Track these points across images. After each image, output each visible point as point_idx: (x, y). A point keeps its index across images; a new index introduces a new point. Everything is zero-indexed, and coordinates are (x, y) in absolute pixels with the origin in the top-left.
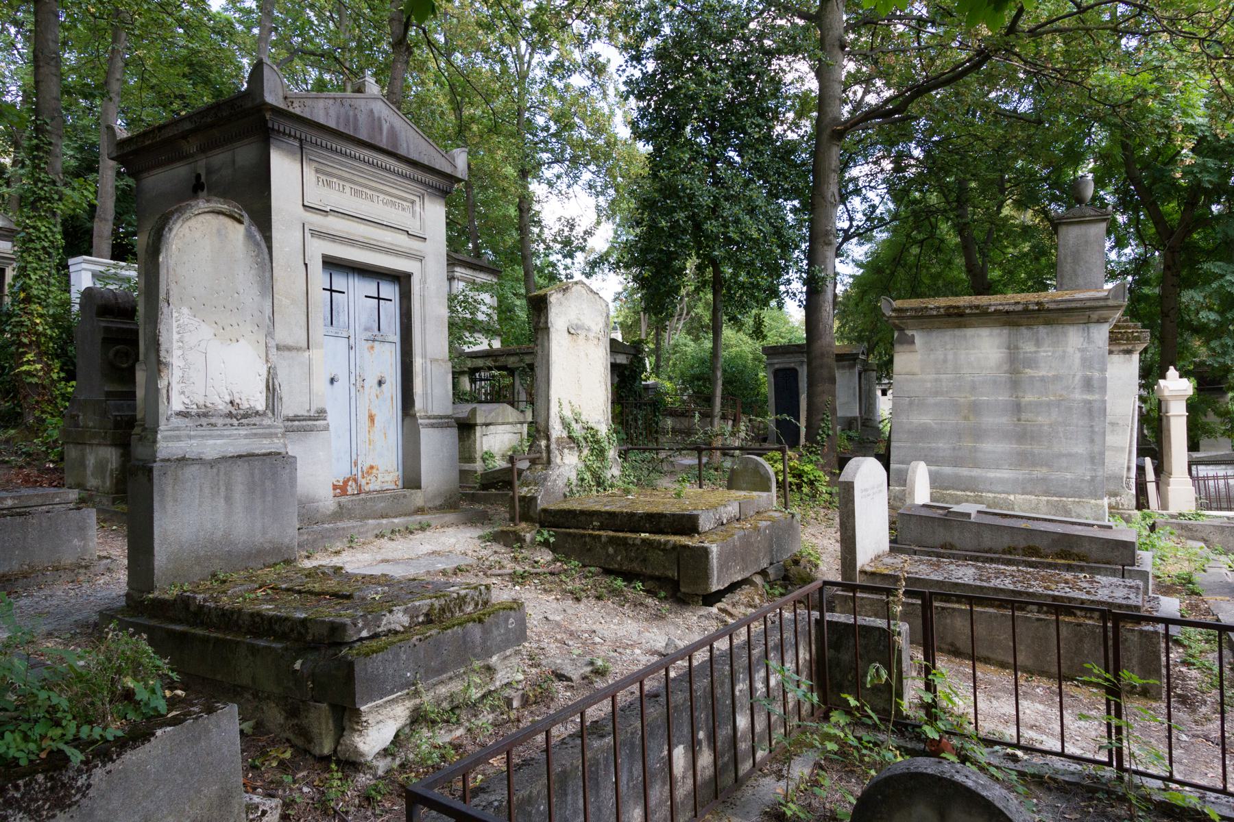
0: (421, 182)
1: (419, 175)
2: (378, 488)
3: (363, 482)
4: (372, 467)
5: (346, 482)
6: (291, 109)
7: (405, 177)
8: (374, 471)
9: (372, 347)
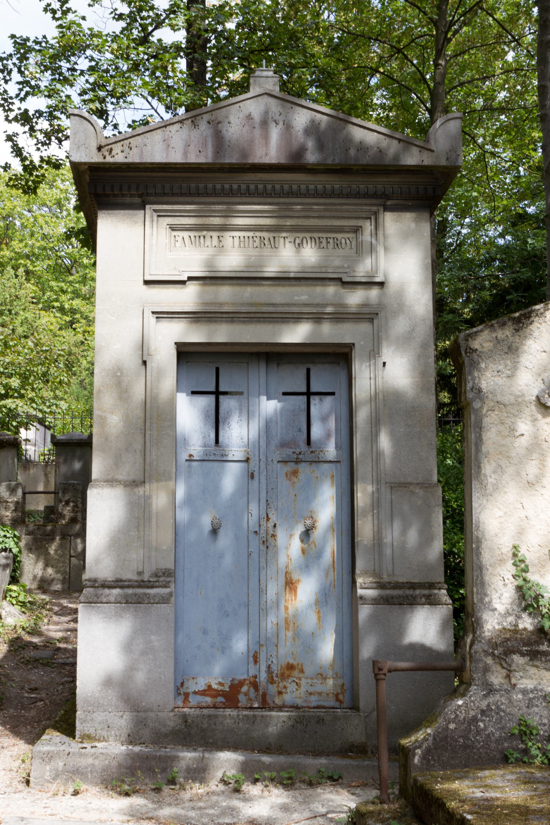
0: (366, 195)
1: (360, 184)
2: (299, 702)
3: (273, 689)
4: (291, 667)
5: (236, 687)
6: (109, 159)
7: (332, 194)
8: (296, 673)
9: (295, 473)
